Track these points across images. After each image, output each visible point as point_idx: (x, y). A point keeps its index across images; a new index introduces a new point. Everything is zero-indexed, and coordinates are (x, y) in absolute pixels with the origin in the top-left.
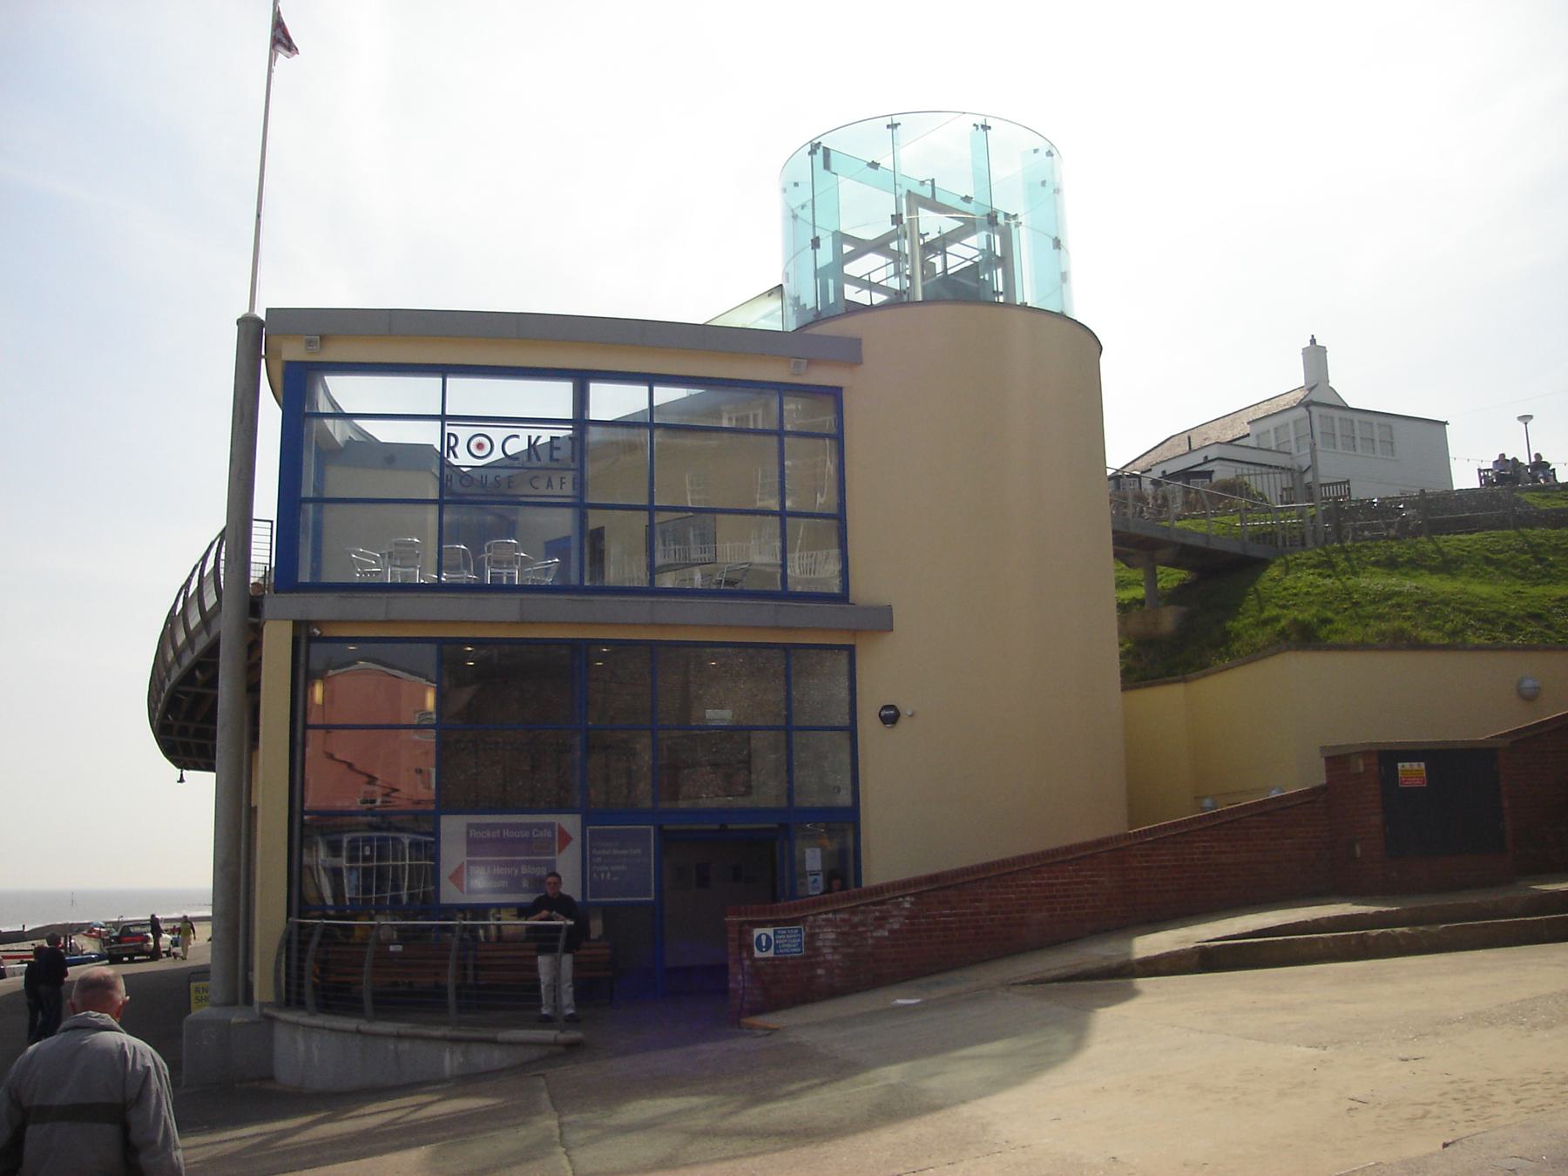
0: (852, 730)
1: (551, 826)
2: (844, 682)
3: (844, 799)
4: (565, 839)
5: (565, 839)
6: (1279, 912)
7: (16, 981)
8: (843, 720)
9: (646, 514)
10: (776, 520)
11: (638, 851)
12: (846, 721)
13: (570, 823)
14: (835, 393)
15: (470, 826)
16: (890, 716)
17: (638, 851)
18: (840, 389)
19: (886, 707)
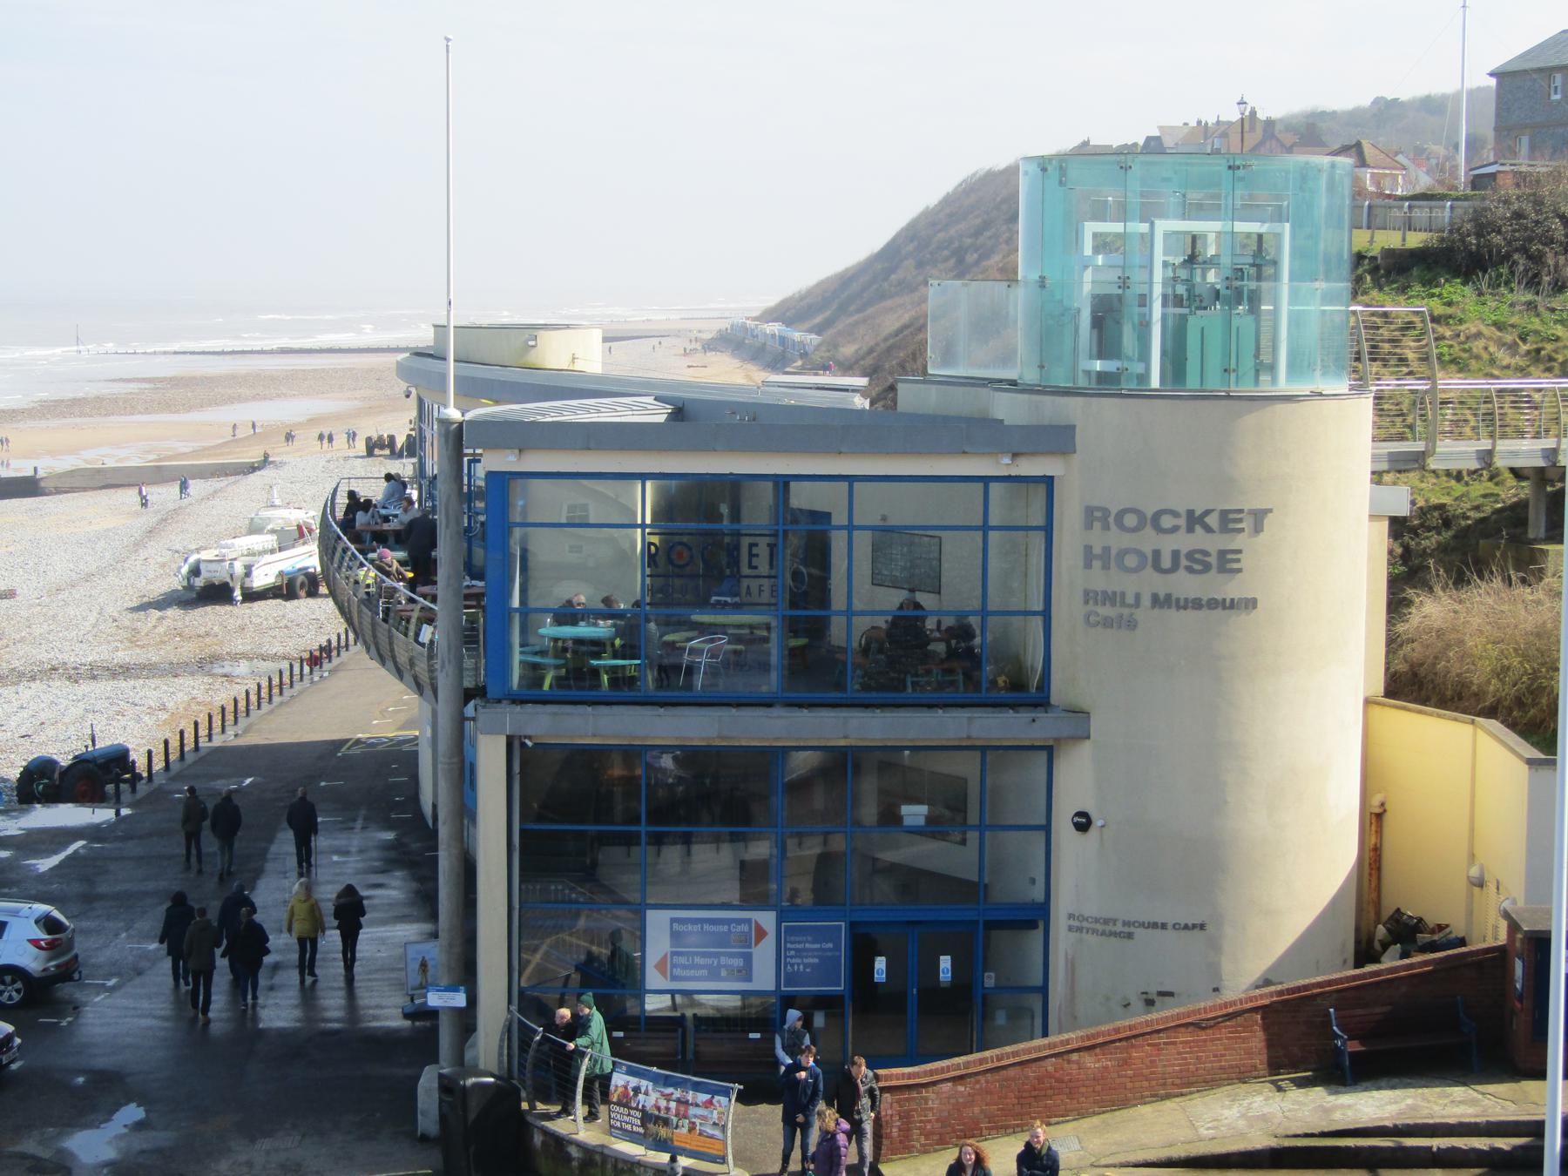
0: (1047, 829)
1: (749, 921)
2: (1044, 770)
3: (1037, 894)
4: (761, 933)
5: (761, 933)
6: (1458, 1092)
7: (14, 774)
8: (1039, 982)
9: (856, 533)
10: (980, 523)
11: (830, 945)
12: (1043, 822)
13: (767, 919)
14: (1049, 481)
15: (673, 920)
16: (1083, 823)
17: (830, 945)
18: (1052, 478)
19: (1079, 814)
